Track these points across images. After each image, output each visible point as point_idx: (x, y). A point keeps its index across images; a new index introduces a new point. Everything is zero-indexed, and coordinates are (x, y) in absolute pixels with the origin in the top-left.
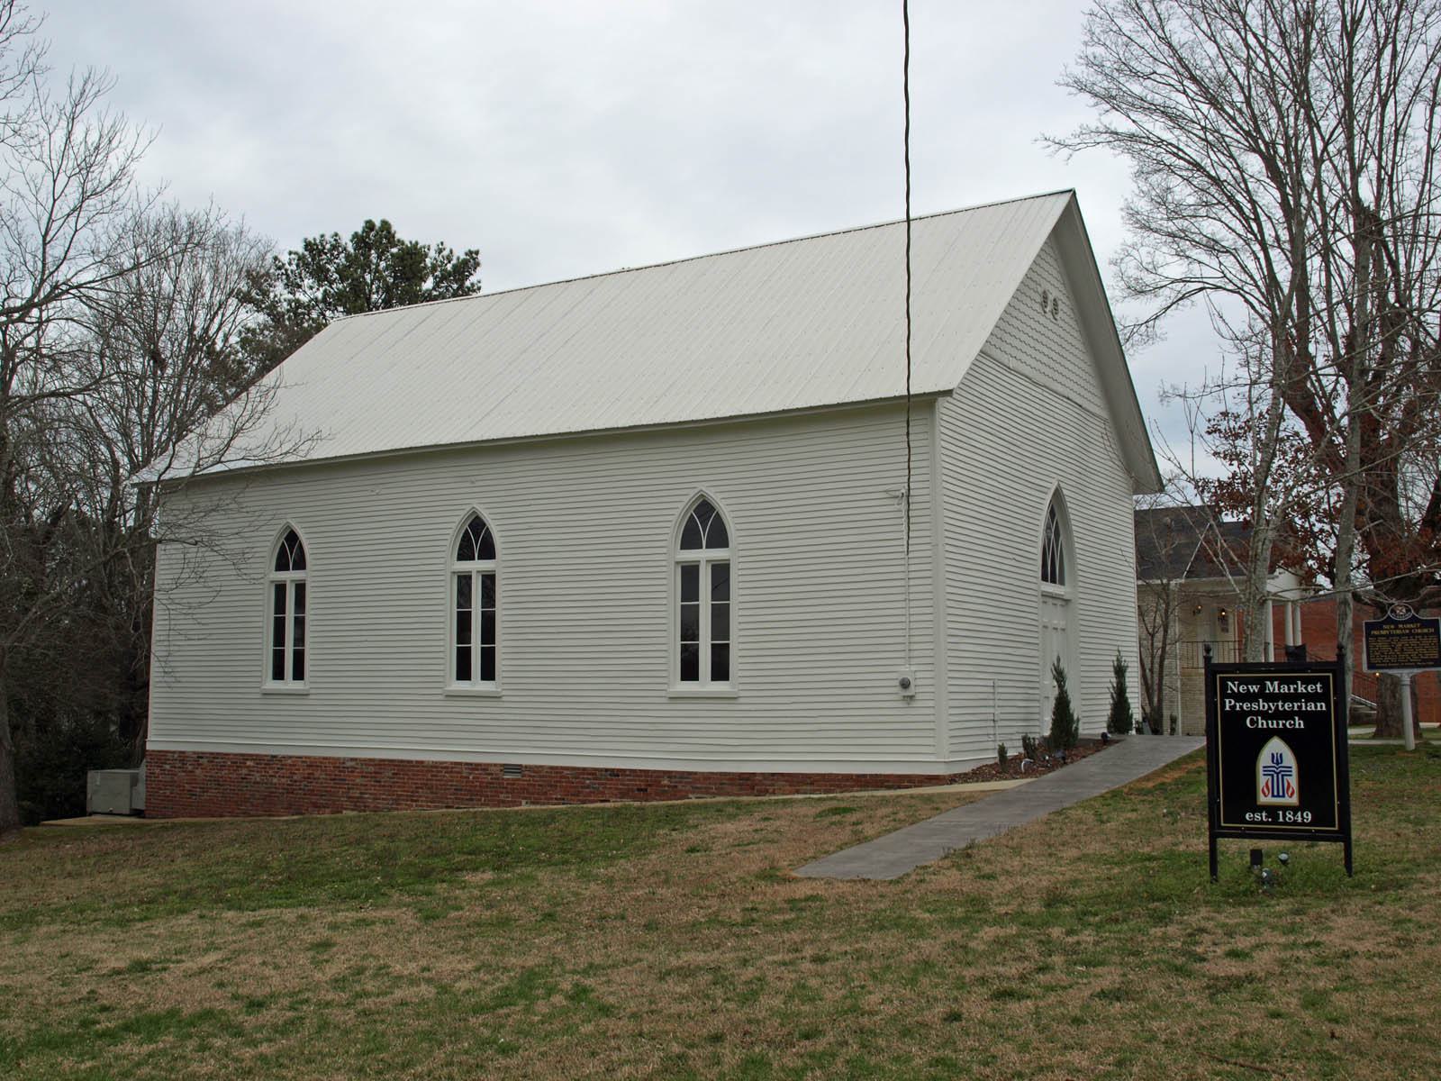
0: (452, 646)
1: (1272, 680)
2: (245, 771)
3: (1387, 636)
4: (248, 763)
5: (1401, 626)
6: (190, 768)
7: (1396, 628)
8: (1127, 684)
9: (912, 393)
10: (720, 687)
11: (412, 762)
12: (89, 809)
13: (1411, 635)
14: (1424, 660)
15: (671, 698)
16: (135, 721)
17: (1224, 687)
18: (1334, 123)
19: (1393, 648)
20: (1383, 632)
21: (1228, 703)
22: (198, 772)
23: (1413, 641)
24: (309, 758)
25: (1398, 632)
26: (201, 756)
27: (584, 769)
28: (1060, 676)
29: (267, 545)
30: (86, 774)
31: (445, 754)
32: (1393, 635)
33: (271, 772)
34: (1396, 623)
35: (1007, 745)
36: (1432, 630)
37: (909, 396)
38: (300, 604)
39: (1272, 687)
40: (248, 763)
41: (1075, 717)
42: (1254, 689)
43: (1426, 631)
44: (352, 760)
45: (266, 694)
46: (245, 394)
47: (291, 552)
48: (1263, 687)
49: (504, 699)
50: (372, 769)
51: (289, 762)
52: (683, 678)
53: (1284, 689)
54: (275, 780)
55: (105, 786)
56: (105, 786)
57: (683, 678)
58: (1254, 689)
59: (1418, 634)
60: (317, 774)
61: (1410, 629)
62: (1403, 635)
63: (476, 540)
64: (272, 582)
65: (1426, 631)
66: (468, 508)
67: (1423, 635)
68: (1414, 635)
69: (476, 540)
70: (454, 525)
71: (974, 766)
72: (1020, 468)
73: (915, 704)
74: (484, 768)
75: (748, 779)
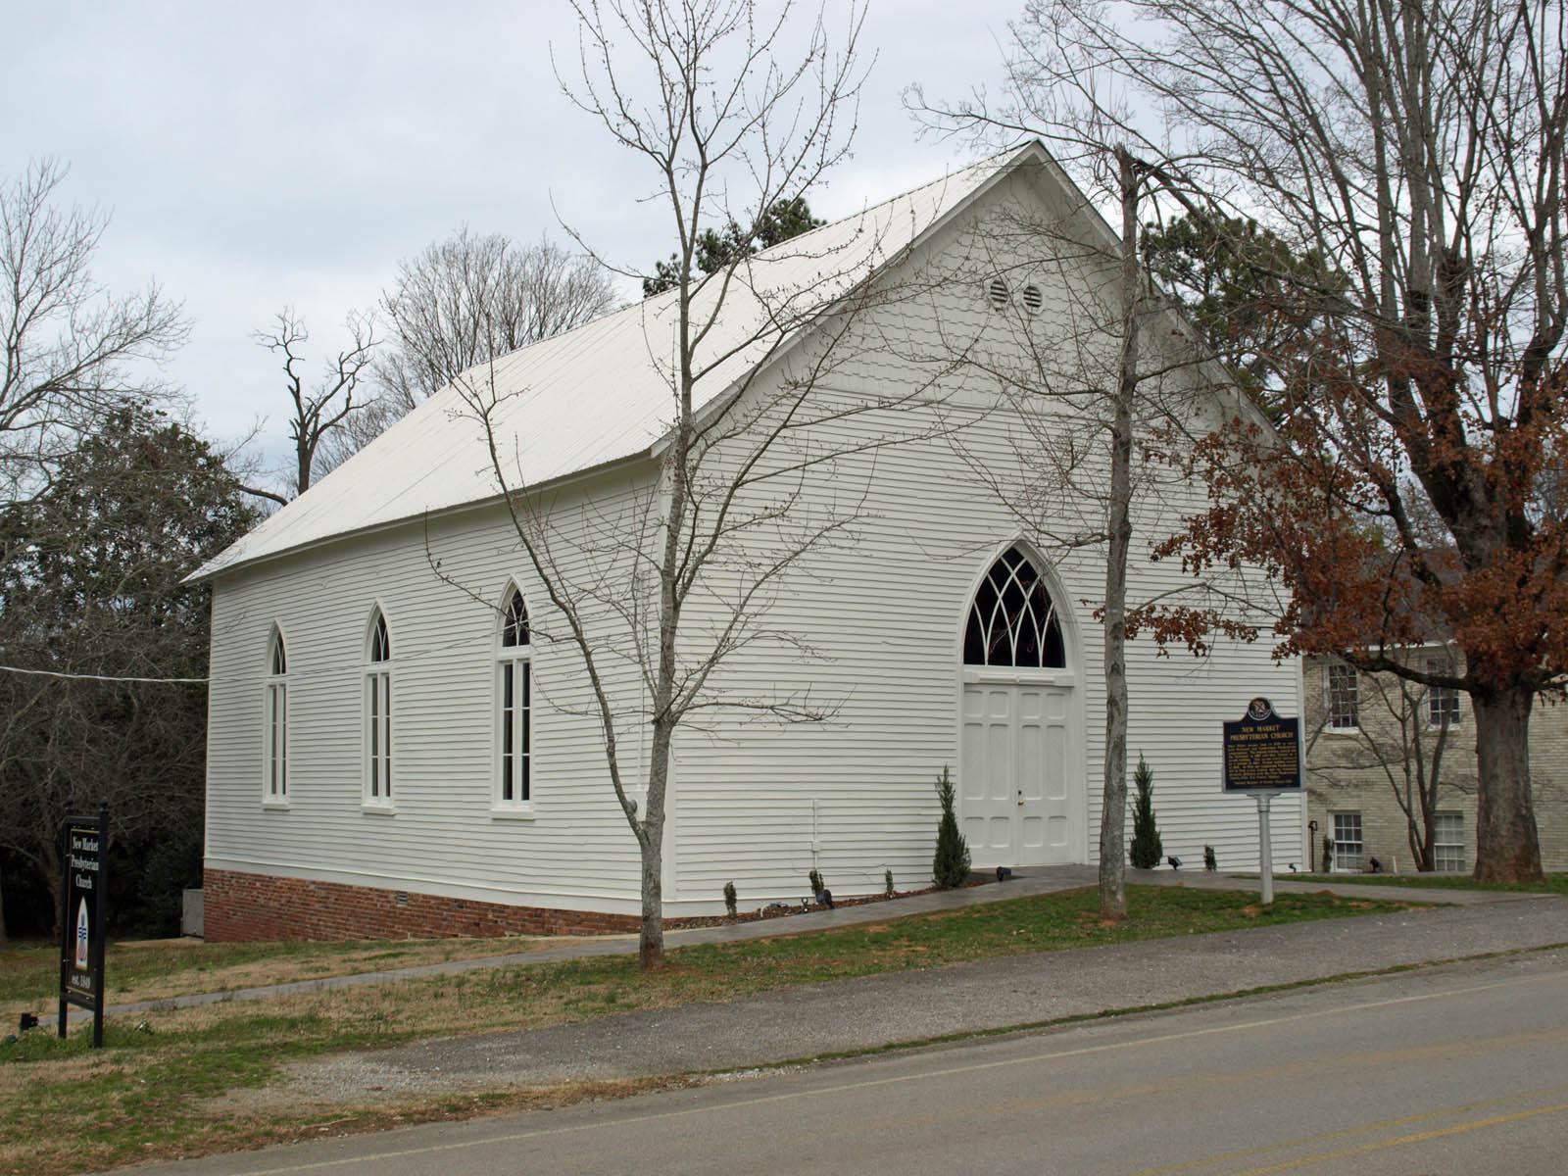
3: (1247, 742)
5: (1259, 729)
7: (1255, 732)
9: (509, 488)
11: (344, 886)
13: (1270, 741)
14: (1283, 777)
15: (495, 819)
19: (1252, 761)
20: (1243, 737)
23: (1272, 750)
24: (289, 879)
25: (1257, 737)
27: (443, 899)
28: (947, 800)
30: (181, 894)
31: (574, 900)
34: (1255, 724)
35: (736, 885)
36: (1291, 735)
37: (507, 494)
40: (258, 884)
43: (1284, 735)
44: (314, 883)
45: (268, 810)
46: (1451, 74)
49: (537, 823)
51: (278, 884)
56: (193, 903)
59: (1278, 740)
61: (1269, 733)
62: (1263, 741)
64: (501, 662)
65: (1284, 735)
67: (1281, 740)
68: (1273, 741)
70: (364, 622)
71: (764, 906)
72: (315, 618)
74: (382, 894)
75: (540, 916)
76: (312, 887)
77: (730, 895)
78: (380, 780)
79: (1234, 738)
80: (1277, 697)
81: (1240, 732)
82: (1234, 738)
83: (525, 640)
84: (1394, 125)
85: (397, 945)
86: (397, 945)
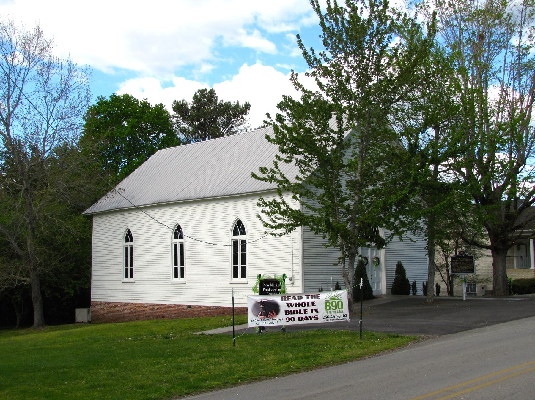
0: (185, 267)
1: (271, 283)
2: (118, 308)
4: (119, 305)
6: (103, 307)
7: (461, 259)
8: (406, 273)
10: (244, 280)
12: (76, 321)
13: (464, 261)
14: (469, 270)
16: (86, 293)
17: (263, 285)
18: (352, 88)
20: (457, 260)
21: (264, 289)
22: (105, 308)
26: (106, 303)
27: (208, 306)
29: (122, 235)
32: (459, 262)
33: (125, 308)
34: (460, 257)
38: (244, 249)
39: (271, 285)
40: (119, 305)
41: (411, 282)
42: (268, 285)
43: (469, 260)
44: (147, 304)
47: (129, 237)
48: (270, 285)
50: (152, 307)
51: (130, 305)
52: (234, 277)
53: (274, 286)
54: (126, 311)
55: (81, 314)
56: (81, 314)
57: (234, 277)
58: (268, 285)
60: (137, 309)
62: (463, 261)
63: (178, 233)
65: (469, 260)
66: (176, 222)
69: (178, 233)
70: (123, 232)
73: (294, 285)
76: (146, 305)
77: (320, 36)
78: (129, 273)
79: (454, 261)
80: (287, 272)
81: (456, 259)
82: (454, 261)
83: (181, 237)
84: (343, 128)
85: (275, 288)
86: (275, 288)
